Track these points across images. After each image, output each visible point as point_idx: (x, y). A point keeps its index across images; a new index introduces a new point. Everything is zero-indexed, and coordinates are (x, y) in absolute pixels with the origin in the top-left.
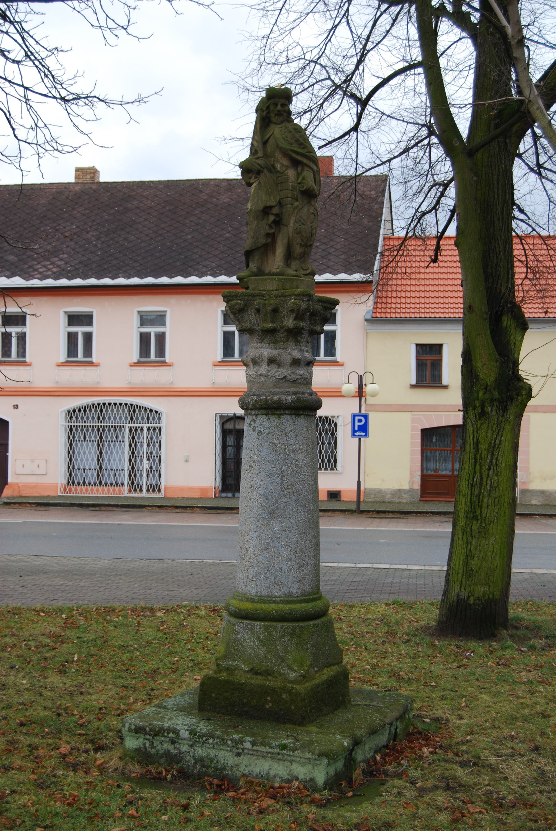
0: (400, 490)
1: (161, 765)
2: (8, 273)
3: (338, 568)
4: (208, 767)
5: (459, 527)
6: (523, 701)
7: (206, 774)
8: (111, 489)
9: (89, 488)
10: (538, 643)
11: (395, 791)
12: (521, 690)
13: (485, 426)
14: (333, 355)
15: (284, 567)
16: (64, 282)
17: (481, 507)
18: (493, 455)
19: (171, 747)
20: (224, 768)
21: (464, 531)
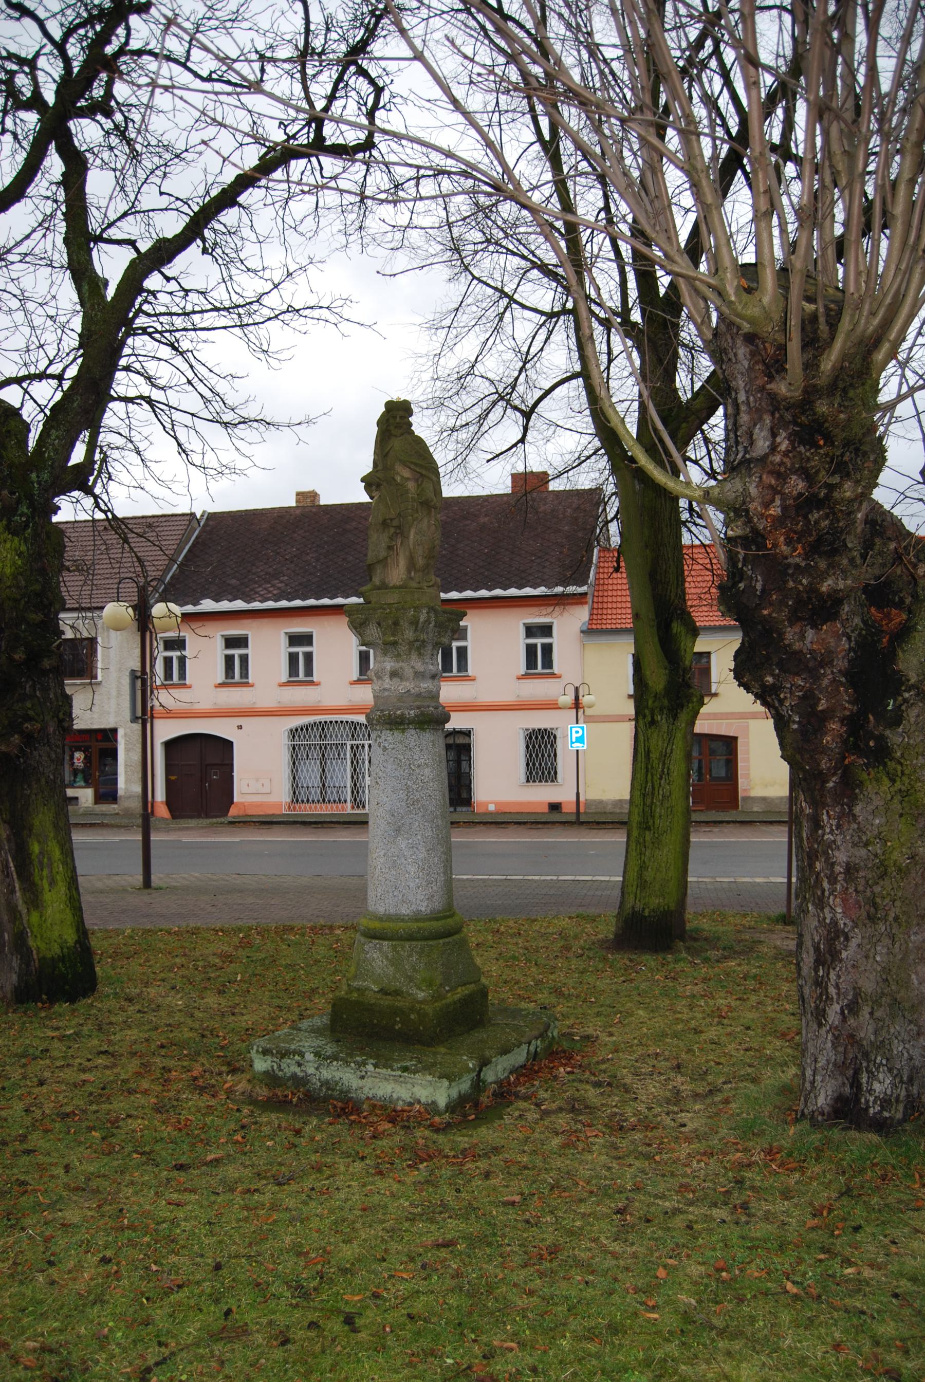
0: (620, 801)
1: (288, 1088)
2: (230, 597)
3: (535, 881)
4: (333, 1090)
5: (633, 839)
6: (679, 1016)
7: (331, 1097)
8: (334, 806)
9: (313, 806)
10: (713, 954)
11: (517, 1114)
12: (681, 1005)
13: (655, 735)
14: (551, 667)
15: (412, 885)
16: (284, 604)
17: (653, 817)
18: (664, 764)
19: (297, 1070)
20: (349, 1091)
21: (638, 842)
